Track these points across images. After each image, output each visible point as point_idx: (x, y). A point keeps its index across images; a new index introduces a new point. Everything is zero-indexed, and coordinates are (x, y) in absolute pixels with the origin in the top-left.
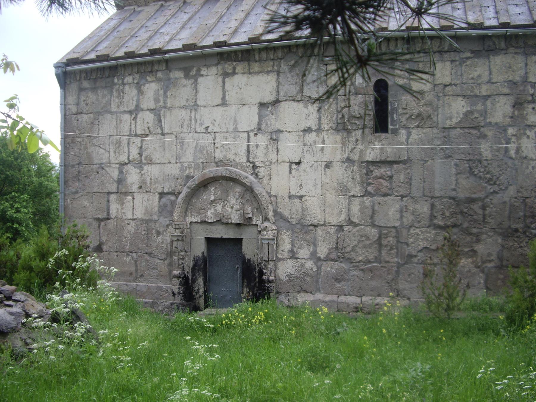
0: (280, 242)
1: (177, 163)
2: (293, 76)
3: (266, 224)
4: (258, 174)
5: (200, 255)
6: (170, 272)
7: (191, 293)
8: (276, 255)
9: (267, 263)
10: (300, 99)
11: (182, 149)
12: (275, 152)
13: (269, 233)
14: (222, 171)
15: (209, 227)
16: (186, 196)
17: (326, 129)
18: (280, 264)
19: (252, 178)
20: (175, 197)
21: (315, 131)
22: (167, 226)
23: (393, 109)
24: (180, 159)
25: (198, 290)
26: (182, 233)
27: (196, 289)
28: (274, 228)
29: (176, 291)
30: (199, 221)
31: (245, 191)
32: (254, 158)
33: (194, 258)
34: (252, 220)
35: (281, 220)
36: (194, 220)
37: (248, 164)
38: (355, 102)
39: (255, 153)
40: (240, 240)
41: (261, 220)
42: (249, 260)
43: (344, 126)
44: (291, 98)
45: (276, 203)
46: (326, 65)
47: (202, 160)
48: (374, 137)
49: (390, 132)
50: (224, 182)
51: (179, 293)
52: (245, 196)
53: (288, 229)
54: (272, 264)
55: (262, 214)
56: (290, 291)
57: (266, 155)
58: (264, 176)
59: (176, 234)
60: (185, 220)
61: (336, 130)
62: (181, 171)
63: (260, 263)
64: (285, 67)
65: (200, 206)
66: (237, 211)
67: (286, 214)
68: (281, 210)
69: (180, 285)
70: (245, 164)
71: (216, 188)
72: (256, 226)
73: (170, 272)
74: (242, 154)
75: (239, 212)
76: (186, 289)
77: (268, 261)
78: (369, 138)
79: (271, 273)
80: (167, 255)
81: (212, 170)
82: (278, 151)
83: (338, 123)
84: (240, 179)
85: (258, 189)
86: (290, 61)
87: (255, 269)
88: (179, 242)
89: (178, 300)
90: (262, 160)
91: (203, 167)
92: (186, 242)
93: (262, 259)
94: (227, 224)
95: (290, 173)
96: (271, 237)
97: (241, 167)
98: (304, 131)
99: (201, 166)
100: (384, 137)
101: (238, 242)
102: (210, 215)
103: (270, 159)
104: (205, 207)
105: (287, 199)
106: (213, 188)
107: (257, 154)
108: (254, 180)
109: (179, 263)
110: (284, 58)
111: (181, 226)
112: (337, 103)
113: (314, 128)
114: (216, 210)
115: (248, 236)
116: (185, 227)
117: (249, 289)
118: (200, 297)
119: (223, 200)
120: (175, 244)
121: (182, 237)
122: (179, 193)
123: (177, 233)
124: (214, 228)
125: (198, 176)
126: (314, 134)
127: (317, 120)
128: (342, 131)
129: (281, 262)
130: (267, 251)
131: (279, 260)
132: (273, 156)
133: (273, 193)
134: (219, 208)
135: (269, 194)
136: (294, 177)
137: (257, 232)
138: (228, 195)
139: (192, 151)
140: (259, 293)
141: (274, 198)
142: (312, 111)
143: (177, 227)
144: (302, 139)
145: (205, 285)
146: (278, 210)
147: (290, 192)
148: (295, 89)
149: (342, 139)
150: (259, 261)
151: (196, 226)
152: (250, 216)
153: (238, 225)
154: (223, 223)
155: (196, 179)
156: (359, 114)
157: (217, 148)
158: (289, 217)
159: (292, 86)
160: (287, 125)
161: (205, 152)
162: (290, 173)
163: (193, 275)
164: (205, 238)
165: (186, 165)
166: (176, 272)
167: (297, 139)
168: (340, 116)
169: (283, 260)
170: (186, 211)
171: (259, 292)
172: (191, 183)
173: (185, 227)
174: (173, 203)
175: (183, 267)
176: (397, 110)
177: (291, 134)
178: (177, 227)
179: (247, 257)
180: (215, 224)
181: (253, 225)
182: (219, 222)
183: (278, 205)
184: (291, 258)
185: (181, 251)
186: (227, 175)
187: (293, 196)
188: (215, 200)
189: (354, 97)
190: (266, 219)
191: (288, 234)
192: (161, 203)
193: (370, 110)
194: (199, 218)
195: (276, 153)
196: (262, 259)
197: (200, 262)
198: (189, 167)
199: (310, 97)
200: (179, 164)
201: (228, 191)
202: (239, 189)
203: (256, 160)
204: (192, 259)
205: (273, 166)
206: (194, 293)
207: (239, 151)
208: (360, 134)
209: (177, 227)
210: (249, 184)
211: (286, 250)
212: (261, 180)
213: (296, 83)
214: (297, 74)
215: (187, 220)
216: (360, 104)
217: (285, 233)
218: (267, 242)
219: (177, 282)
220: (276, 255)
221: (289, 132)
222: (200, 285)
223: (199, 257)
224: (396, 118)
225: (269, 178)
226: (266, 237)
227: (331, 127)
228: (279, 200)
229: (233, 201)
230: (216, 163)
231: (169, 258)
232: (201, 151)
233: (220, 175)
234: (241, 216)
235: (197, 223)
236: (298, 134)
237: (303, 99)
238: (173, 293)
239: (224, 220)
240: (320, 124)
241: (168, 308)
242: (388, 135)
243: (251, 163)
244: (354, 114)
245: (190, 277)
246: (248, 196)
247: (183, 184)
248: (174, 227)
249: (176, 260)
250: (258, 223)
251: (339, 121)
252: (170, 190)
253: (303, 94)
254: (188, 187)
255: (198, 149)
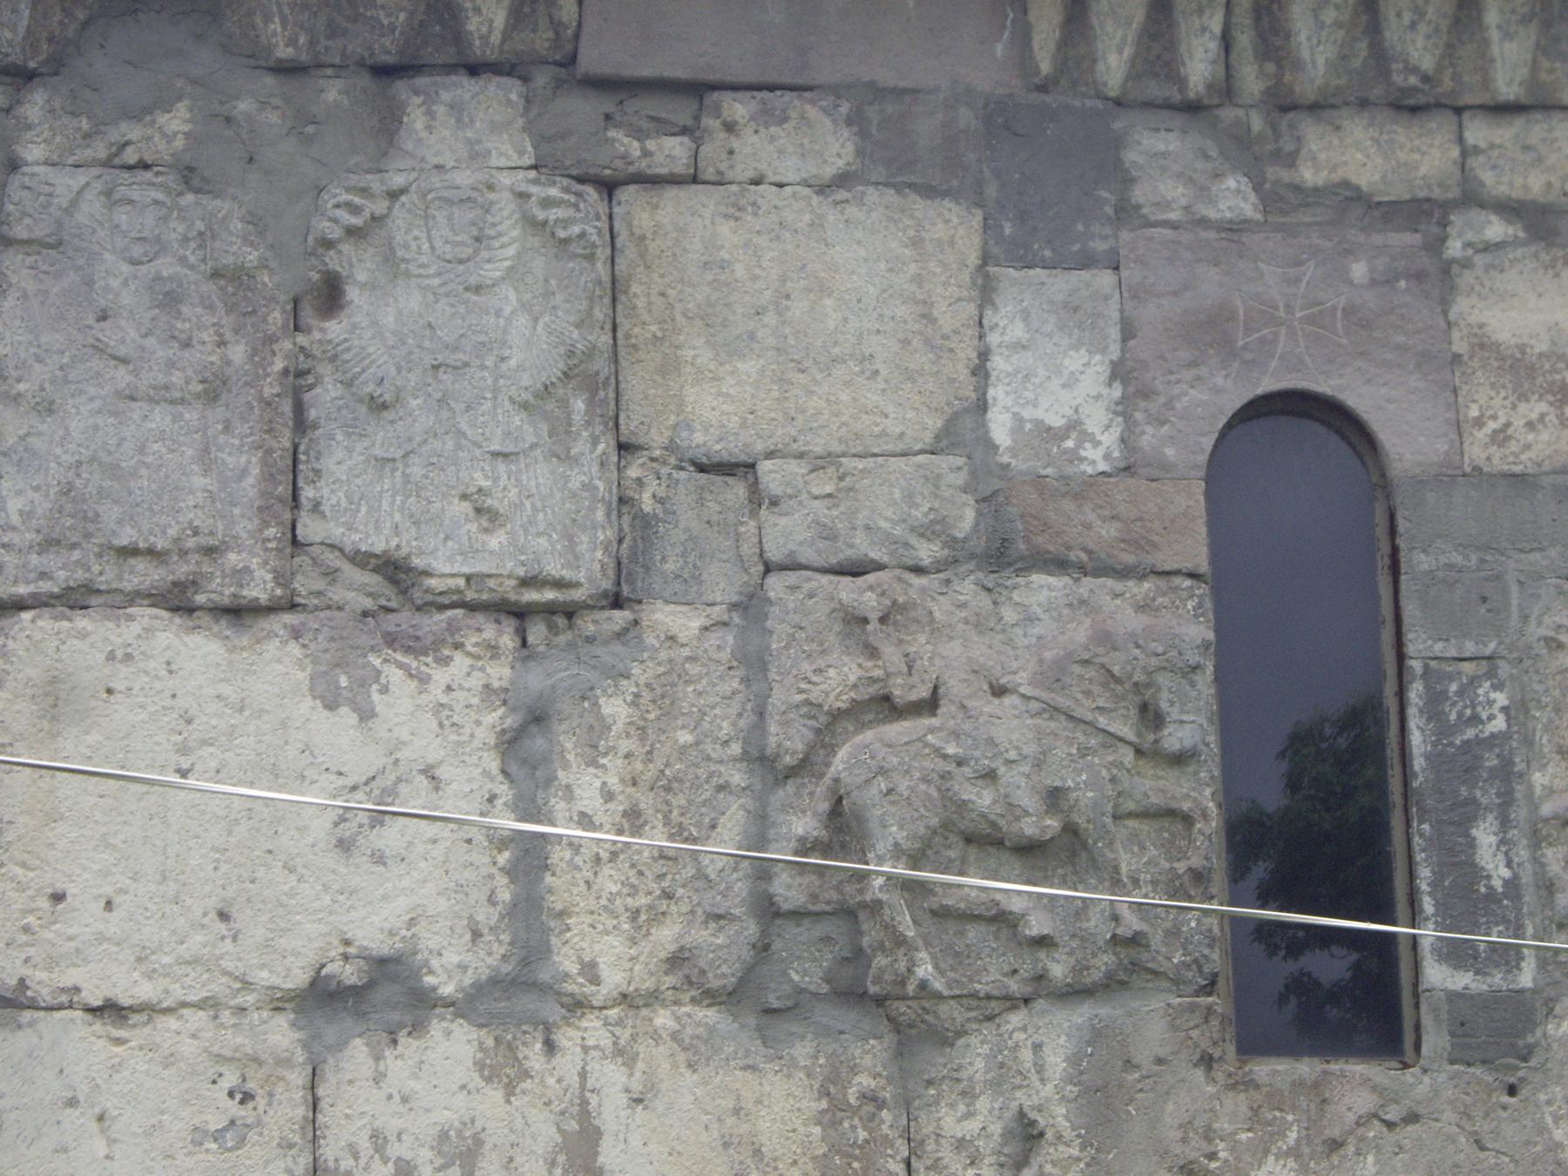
2: (169, 299)
10: (260, 588)
17: (613, 979)
21: (467, 1006)
23: (1461, 762)
38: (981, 650)
43: (857, 957)
44: (144, 574)
46: (609, 188)
48: (1239, 1103)
49: (1435, 1040)
61: (753, 999)
64: (67, 183)
78: (1172, 1113)
83: (768, 911)
86: (140, 113)
98: (323, 999)
100: (1363, 1101)
110: (56, 66)
112: (754, 665)
113: (450, 965)
126: (452, 1046)
127: (487, 876)
128: (829, 1015)
142: (426, 745)
144: (286, 1110)
148: (206, 458)
149: (831, 1118)
156: (1054, 797)
159: (160, 418)
160: (84, 918)
167: (219, 1110)
168: (804, 825)
176: (1506, 774)
177: (137, 1035)
189: (966, 588)
192: (506, 48)
193: (1179, 759)
199: (395, 571)
208: (1056, 1062)
210: (1334, 948)
213: (213, 389)
214: (232, 279)
216: (1053, 675)
221: (111, 1011)
224: (1499, 873)
227: (676, 960)
236: (234, 1040)
237: (304, 584)
240: (529, 914)
242: (1417, 1084)
244: (983, 799)
251: (788, 891)
253: (309, 528)
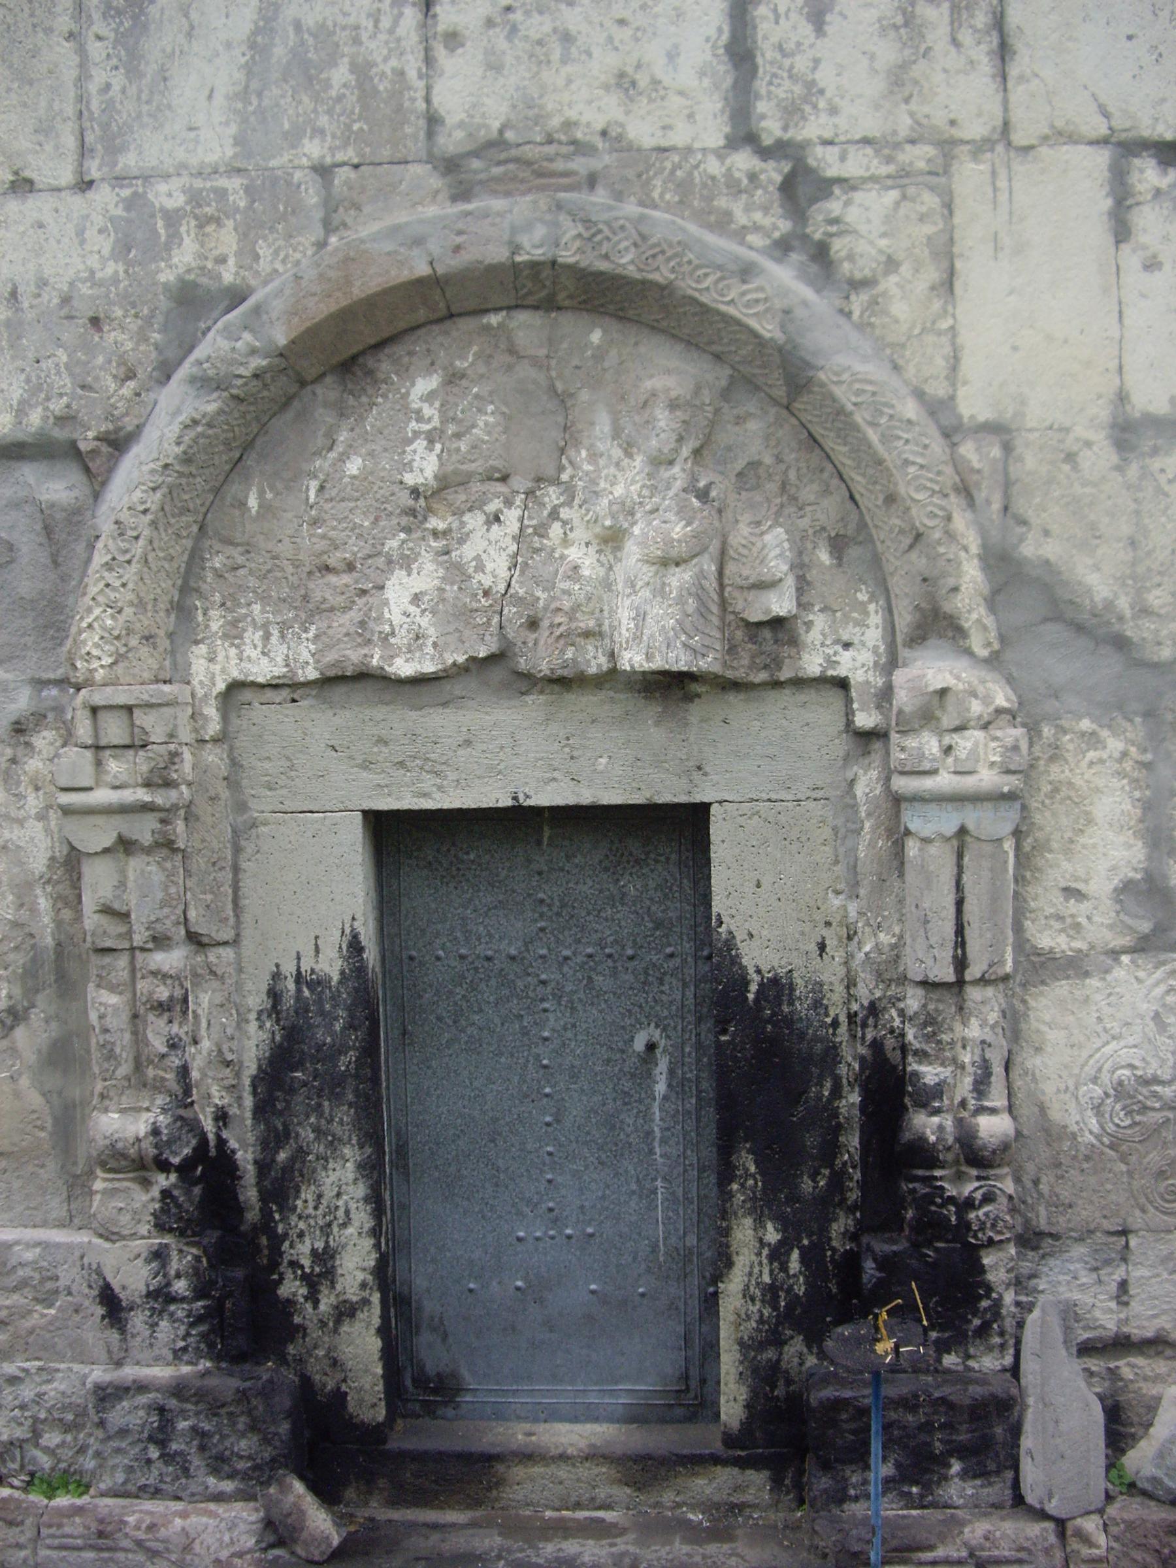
0: (1050, 822)
1: (85, 185)
3: (933, 669)
4: (838, 247)
5: (331, 965)
6: (67, 1122)
7: (261, 1287)
8: (1018, 928)
9: (946, 1007)
11: (132, 65)
12: (981, 54)
13: (965, 743)
14: (519, 227)
15: (397, 720)
16: (187, 459)
18: (1047, 1007)
19: (785, 278)
20: (75, 475)
22: (19, 729)
24: (114, 149)
25: (326, 1258)
26: (160, 780)
27: (303, 1251)
28: (1001, 701)
29: (133, 1278)
30: (312, 674)
31: (725, 394)
32: (792, 112)
33: (274, 995)
34: (794, 641)
35: (1053, 631)
36: (263, 670)
37: (743, 161)
39: (801, 63)
40: (699, 814)
41: (873, 635)
42: (777, 988)
45: (1007, 485)
47: (313, 149)
50: (526, 326)
51: (161, 1297)
52: (727, 435)
53: (1112, 709)
54: (986, 1005)
55: (883, 589)
56: (1136, 1220)
57: (899, 81)
58: (891, 264)
59: (102, 796)
60: (179, 674)
62: (123, 249)
63: (874, 1009)
65: (310, 543)
66: (666, 562)
67: (1097, 580)
68: (1051, 550)
69: (161, 1227)
70: (713, 167)
71: (453, 378)
72: (834, 698)
73: (67, 1122)
74: (686, 76)
75: (678, 579)
76: (220, 1256)
77: (960, 983)
79: (981, 1086)
80: (30, 978)
81: (412, 230)
82: (1004, 51)
84: (688, 286)
85: (848, 364)
87: (832, 1054)
88: (135, 865)
89: (159, 1359)
90: (871, 125)
91: (330, 206)
92: (199, 863)
93: (890, 971)
94: (565, 682)
95: (1121, 231)
96: (986, 778)
97: (684, 188)
99: (311, 196)
101: (680, 830)
102: (410, 615)
103: (939, 119)
104: (354, 548)
105: (1100, 457)
106: (425, 385)
107: (825, 77)
108: (808, 293)
109: (138, 1037)
111: (153, 724)
114: (457, 572)
115: (754, 781)
116: (185, 735)
117: (784, 1223)
118: (346, 1311)
119: (520, 483)
120: (99, 882)
121: (166, 814)
122: (118, 442)
123: (119, 782)
124: (441, 723)
125: (286, 282)
129: (1061, 988)
130: (949, 901)
131: (1040, 967)
132: (961, 93)
133: (973, 406)
134: (489, 550)
135: (942, 414)
136: (1152, 265)
137: (842, 745)
138: (569, 437)
139: (226, 74)
140: (884, 1263)
141: (986, 453)
143: (122, 730)
145: (375, 1200)
146: (1028, 550)
147: (1122, 397)
150: (866, 991)
151: (273, 720)
152: (781, 604)
153: (670, 687)
154: (528, 682)
155: (278, 306)
157: (453, 39)
158: (1123, 604)
161: (340, 75)
162: (1121, 231)
163: (272, 1140)
164: (366, 813)
165: (168, 195)
166: (126, 1123)
169: (1074, 966)
170: (186, 589)
171: (882, 1247)
172: (221, 345)
173: (185, 735)
174: (63, 534)
175: (184, 1072)
178: (122, 730)
179: (759, 957)
180: (457, 688)
181: (799, 683)
182: (496, 670)
183: (1020, 506)
184: (1143, 946)
185: (160, 941)
186: (567, 256)
187: (1154, 422)
188: (445, 484)
190: (935, 625)
191: (1115, 745)
194: (305, 651)
195: (986, 66)
196: (890, 971)
197: (333, 1026)
198: (204, 212)
200: (105, 197)
201: (563, 400)
202: (666, 375)
203: (812, 129)
204: (256, 999)
205: (969, 175)
206: (291, 1287)
207: (654, 52)
209: (114, 730)
210: (768, 329)
211: (1101, 886)
212: (858, 301)
215: (199, 666)
217: (1092, 740)
218: (946, 822)
219: (135, 1203)
220: (1018, 928)
222: (336, 1215)
223: (317, 983)
225: (933, 274)
226: (944, 781)
228: (1030, 462)
229: (625, 482)
230: (450, 166)
231: (44, 1003)
232: (306, 73)
233: (497, 254)
234: (703, 611)
235: (287, 687)
238: (112, 1305)
239: (543, 657)
241: (67, 1428)
243: (765, 153)
245: (245, 1158)
246: (753, 434)
247: (146, 358)
248: (83, 730)
249: (119, 1022)
250: (849, 664)
252: (35, 418)
254: (203, 383)
255: (279, 52)
